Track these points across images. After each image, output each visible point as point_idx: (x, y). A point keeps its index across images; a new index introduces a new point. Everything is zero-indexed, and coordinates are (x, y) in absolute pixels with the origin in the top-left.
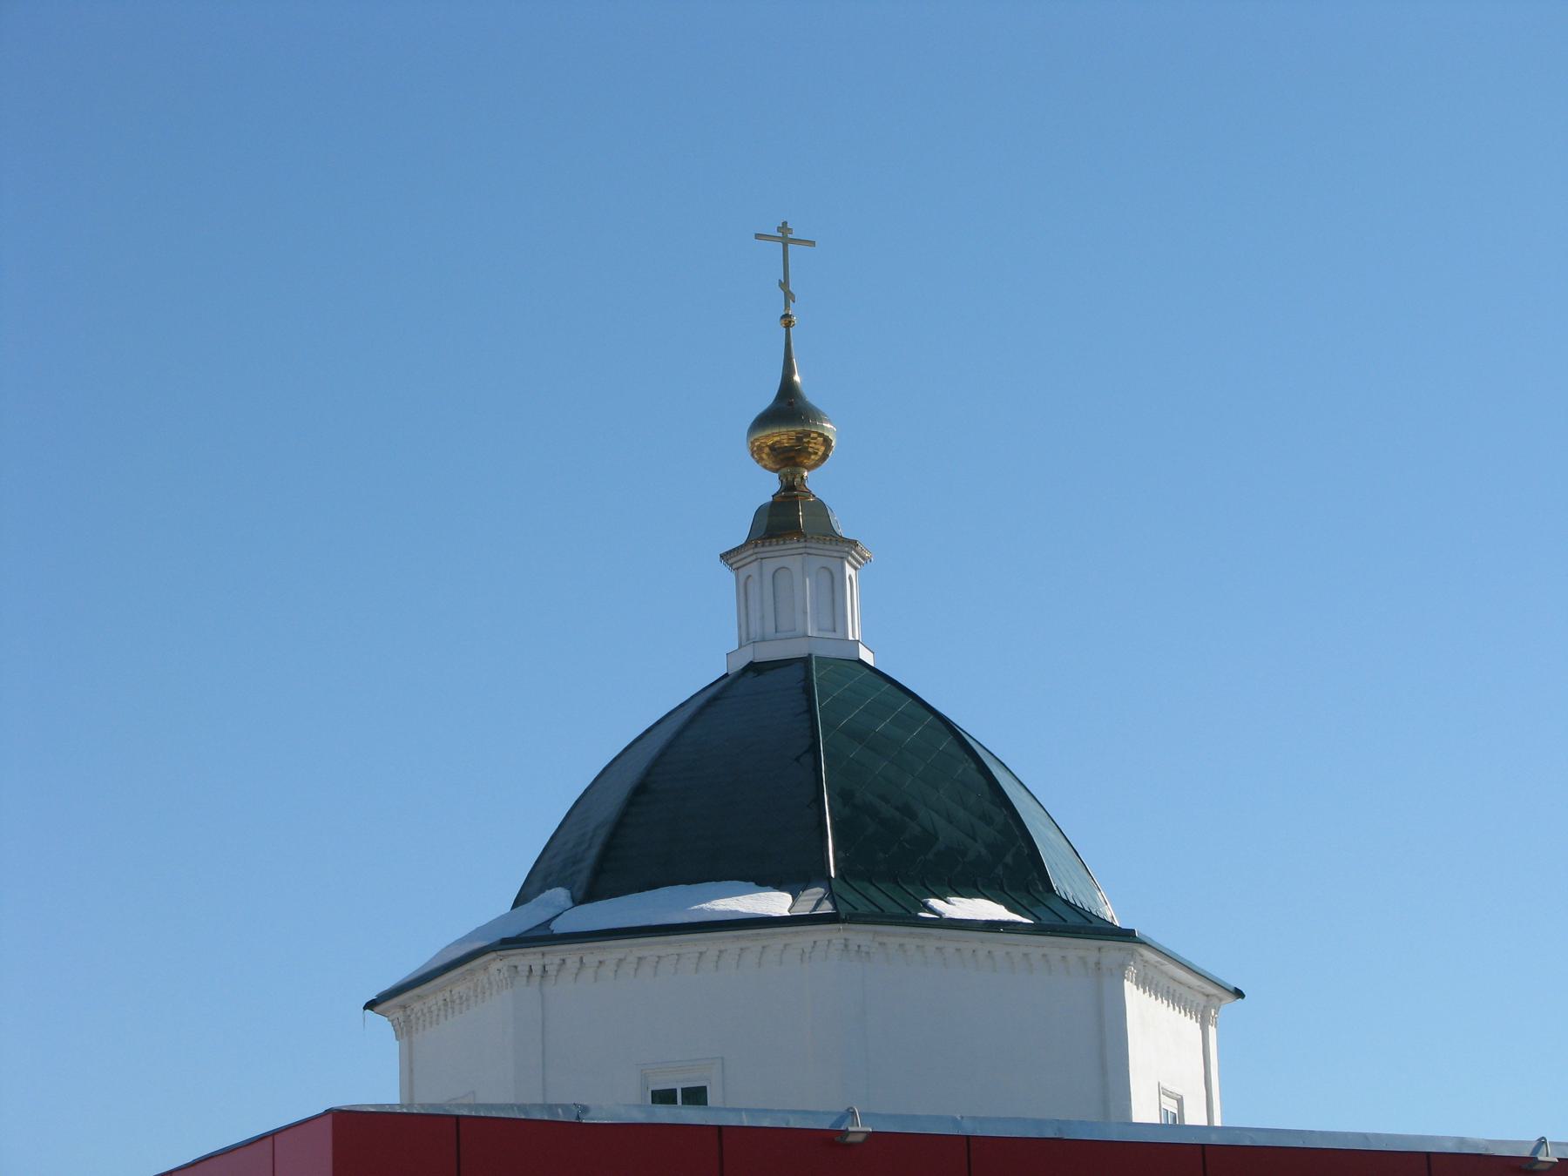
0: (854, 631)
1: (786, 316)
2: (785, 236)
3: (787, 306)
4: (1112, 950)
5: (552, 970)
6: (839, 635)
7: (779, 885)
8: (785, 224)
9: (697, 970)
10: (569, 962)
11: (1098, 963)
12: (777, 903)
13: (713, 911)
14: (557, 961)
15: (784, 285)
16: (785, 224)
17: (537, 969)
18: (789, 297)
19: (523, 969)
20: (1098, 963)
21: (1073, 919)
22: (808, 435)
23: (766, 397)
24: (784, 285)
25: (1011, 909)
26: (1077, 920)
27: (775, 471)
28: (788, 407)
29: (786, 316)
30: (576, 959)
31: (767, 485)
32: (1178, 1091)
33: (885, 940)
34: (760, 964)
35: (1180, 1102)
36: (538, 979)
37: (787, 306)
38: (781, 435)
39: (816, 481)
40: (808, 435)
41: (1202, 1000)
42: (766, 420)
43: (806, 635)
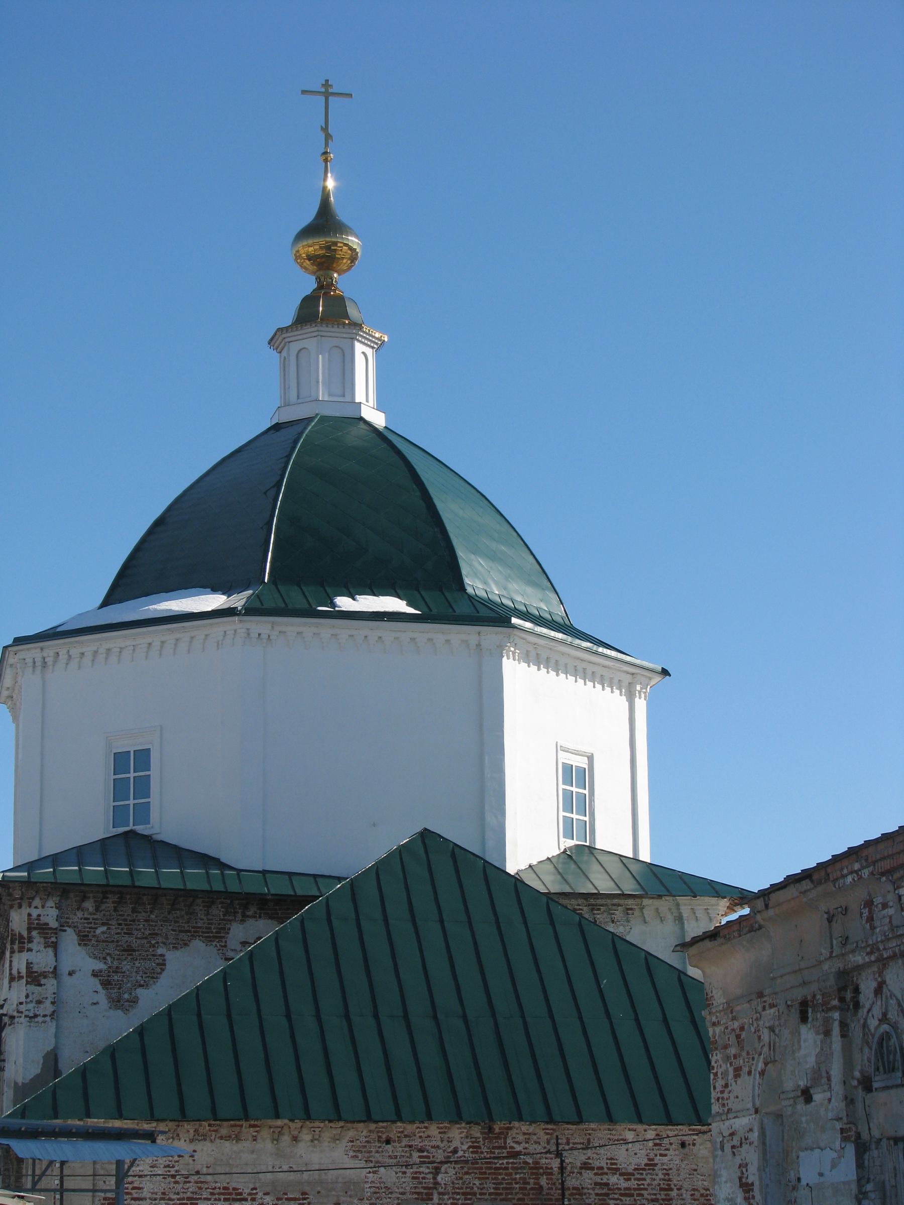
0: (360, 397)
1: (326, 153)
2: (327, 91)
3: (327, 145)
4: (490, 635)
5: (49, 660)
6: (347, 399)
7: (215, 589)
8: (327, 81)
9: (146, 657)
10: (60, 654)
11: (478, 645)
12: (214, 601)
13: (156, 610)
14: (52, 653)
15: (325, 129)
16: (327, 81)
17: (39, 660)
18: (328, 137)
19: (29, 661)
20: (478, 645)
21: (484, 612)
22: (335, 244)
23: (309, 215)
24: (325, 129)
25: (409, 605)
26: (492, 614)
27: (314, 273)
28: (325, 222)
29: (326, 153)
30: (65, 652)
31: (309, 284)
32: (589, 750)
33: (284, 629)
34: (189, 651)
35: (591, 758)
36: (31, 669)
37: (327, 145)
38: (312, 246)
39: (343, 283)
40: (335, 244)
41: (627, 679)
42: (308, 232)
43: (322, 398)
